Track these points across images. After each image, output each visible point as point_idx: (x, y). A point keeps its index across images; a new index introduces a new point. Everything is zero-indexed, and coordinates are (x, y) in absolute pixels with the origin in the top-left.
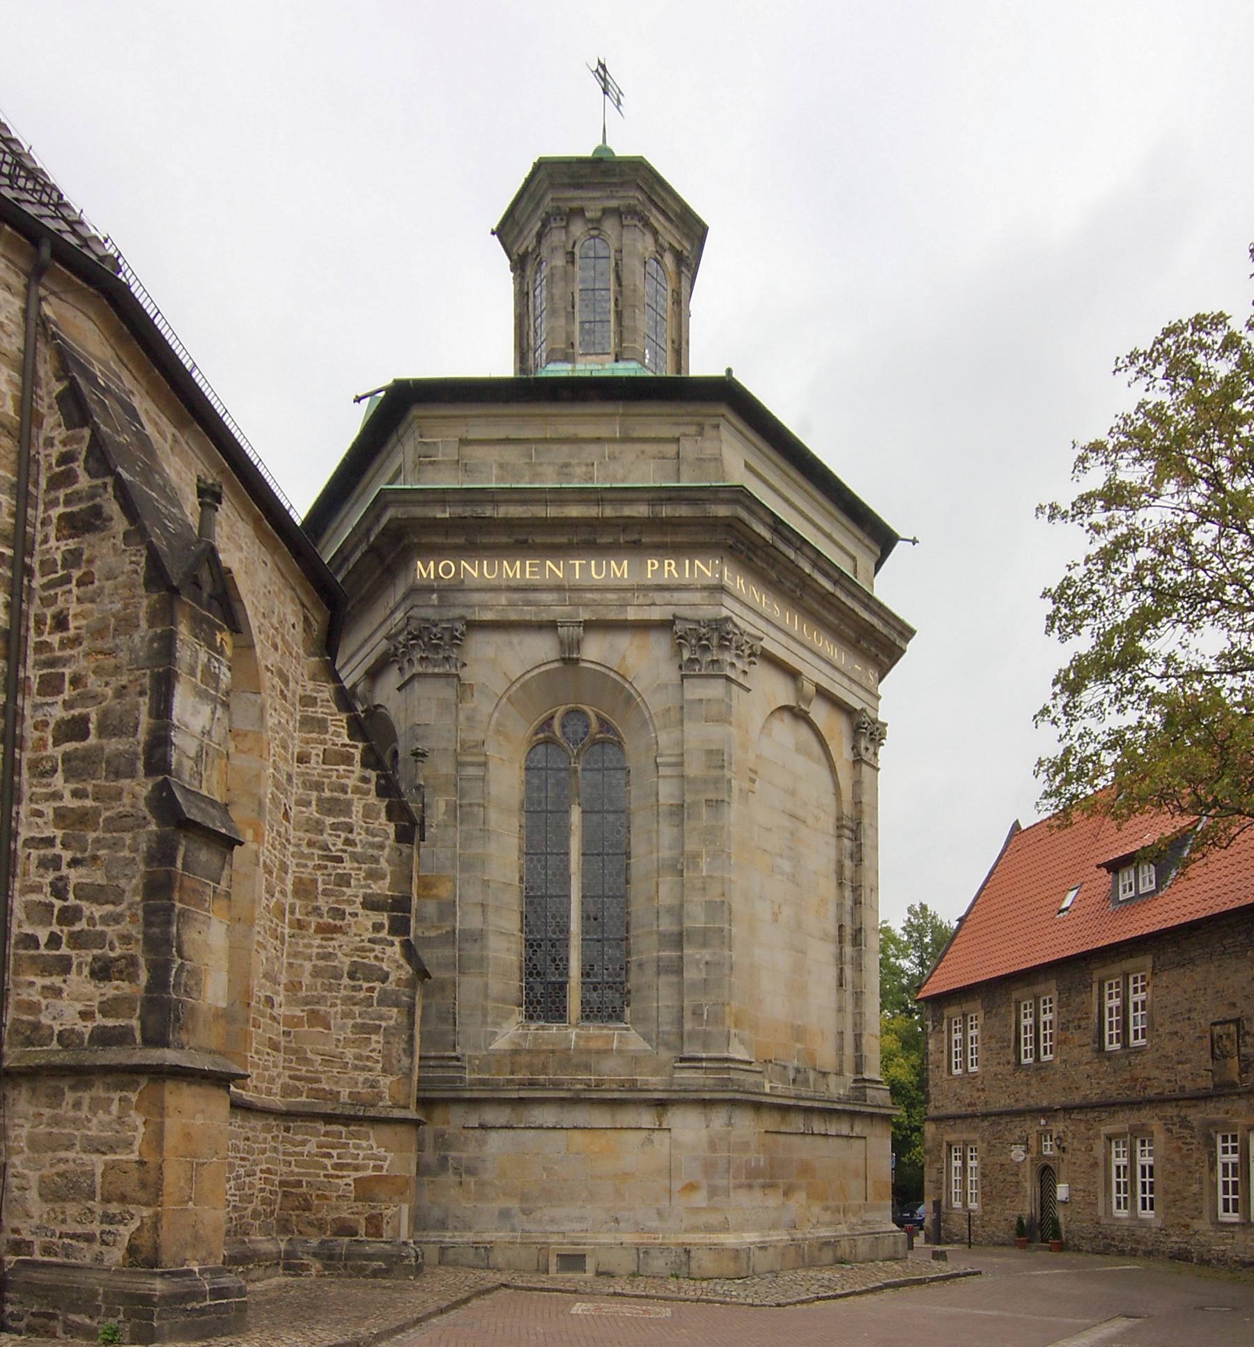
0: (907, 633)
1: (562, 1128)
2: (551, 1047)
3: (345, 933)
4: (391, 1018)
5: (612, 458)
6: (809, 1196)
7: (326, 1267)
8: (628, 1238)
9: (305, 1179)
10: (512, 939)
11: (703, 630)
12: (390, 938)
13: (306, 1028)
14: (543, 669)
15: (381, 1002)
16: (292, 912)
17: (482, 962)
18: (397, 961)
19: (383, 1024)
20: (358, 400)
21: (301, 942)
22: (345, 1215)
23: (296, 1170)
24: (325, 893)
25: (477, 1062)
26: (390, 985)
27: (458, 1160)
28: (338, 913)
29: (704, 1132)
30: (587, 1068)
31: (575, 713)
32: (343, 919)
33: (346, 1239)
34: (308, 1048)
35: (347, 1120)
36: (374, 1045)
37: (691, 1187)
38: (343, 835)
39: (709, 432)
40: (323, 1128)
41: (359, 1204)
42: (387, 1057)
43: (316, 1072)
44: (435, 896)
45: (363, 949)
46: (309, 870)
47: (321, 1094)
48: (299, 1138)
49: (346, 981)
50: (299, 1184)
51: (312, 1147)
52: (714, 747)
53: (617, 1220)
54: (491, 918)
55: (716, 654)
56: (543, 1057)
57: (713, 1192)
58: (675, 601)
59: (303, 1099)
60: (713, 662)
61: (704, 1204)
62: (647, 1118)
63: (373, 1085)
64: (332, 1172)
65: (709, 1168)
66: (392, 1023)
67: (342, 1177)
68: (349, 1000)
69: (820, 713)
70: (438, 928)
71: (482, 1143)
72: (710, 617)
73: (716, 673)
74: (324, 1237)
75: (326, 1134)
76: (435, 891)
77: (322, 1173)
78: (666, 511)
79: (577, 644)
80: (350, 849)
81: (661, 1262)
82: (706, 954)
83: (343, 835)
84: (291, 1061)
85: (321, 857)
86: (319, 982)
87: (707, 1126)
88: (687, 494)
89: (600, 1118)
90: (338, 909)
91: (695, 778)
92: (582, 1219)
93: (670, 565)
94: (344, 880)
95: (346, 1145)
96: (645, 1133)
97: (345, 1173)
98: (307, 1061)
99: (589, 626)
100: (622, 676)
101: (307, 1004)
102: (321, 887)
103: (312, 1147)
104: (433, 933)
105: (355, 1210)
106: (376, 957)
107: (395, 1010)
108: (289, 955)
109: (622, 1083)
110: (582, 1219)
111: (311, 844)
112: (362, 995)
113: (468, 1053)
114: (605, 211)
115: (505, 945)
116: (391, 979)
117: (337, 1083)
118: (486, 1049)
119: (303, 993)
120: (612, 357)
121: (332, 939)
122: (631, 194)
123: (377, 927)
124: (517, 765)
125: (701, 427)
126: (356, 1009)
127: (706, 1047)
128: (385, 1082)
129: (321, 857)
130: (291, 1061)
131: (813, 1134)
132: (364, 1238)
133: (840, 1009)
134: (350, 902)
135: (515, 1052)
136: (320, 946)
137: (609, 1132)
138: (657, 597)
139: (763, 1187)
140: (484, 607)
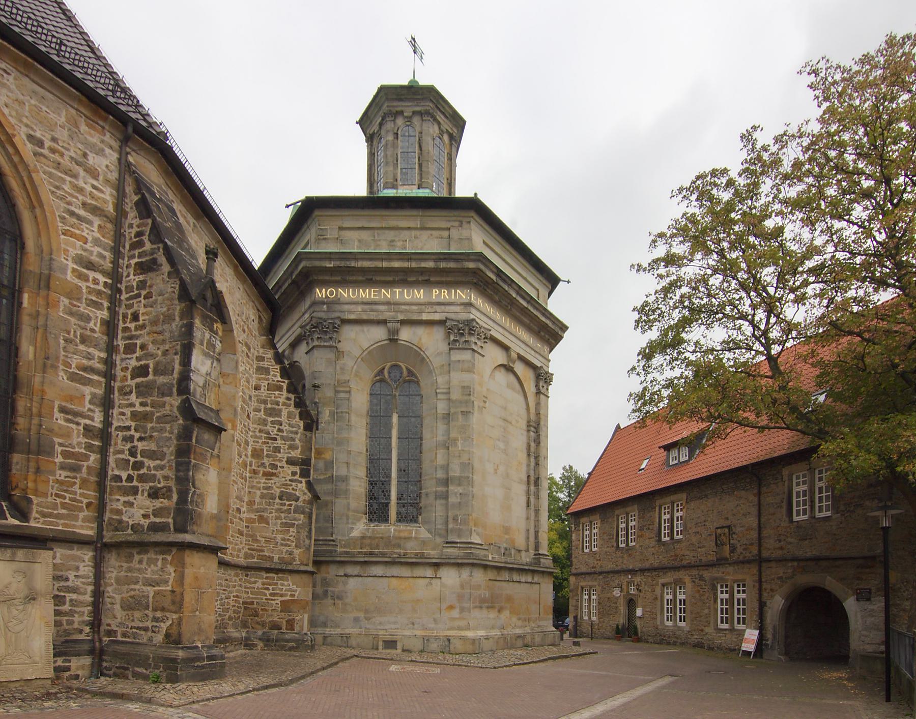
0: (564, 328)
5: (416, 237)
6: (511, 613)
16: (251, 465)
17: (346, 492)
20: (287, 206)
24: (268, 456)
26: (300, 503)
27: (333, 592)
28: (274, 466)
29: (458, 579)
30: (399, 546)
34: (258, 534)
35: (278, 571)
37: (451, 607)
40: (265, 575)
42: (298, 539)
44: (324, 458)
45: (286, 485)
48: (253, 580)
49: (277, 500)
50: (252, 603)
51: (259, 584)
54: (352, 469)
55: (467, 338)
57: (462, 610)
59: (255, 560)
60: (466, 341)
61: (457, 616)
62: (429, 572)
65: (460, 597)
66: (301, 522)
69: (519, 368)
71: (345, 584)
75: (267, 578)
78: (443, 265)
79: (397, 332)
85: (266, 438)
86: (264, 501)
89: (405, 572)
94: (277, 450)
99: (403, 322)
102: (265, 453)
103: (259, 584)
104: (322, 477)
109: (417, 554)
110: (395, 623)
111: (260, 431)
112: (286, 508)
113: (339, 538)
114: (414, 113)
115: (359, 483)
119: (256, 507)
123: (294, 474)
125: (461, 222)
126: (283, 515)
127: (459, 536)
128: (297, 552)
129: (266, 438)
134: (280, 461)
135: (363, 538)
137: (410, 579)
138: (438, 308)
140: (350, 312)
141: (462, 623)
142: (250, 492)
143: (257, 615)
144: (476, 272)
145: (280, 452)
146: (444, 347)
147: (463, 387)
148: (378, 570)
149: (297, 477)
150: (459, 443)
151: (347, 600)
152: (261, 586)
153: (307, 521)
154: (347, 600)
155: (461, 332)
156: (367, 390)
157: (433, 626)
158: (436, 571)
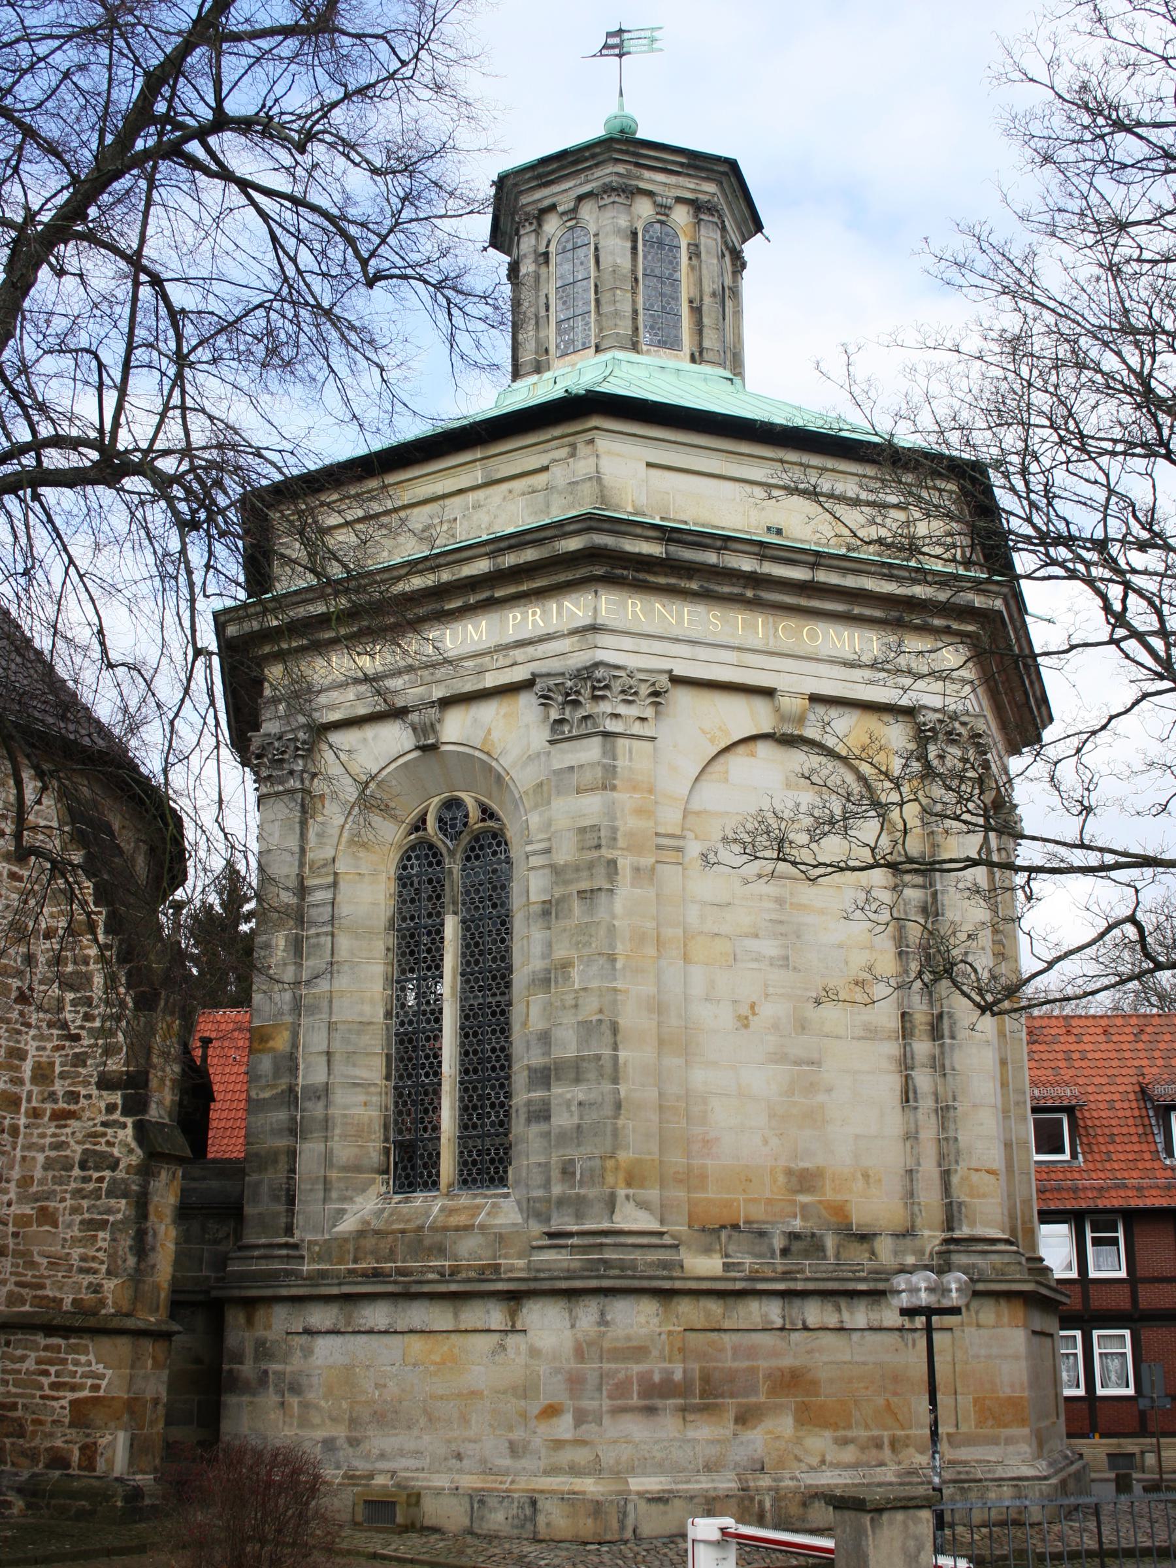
1: (395, 1332)
2: (401, 1226)
3: (79, 1119)
4: (119, 1211)
5: (477, 506)
6: (800, 1422)
7: (29, 1506)
8: (469, 1482)
9: (20, 1401)
10: (372, 1089)
11: (569, 684)
12: (123, 1119)
13: (35, 1228)
14: (401, 761)
15: (110, 1194)
16: (29, 1100)
17: (326, 1124)
18: (128, 1145)
19: (111, 1219)
21: (36, 1132)
22: (59, 1443)
23: (14, 1390)
24: (62, 1076)
25: (317, 1248)
26: (120, 1174)
27: (280, 1375)
28: (73, 1097)
29: (568, 1333)
30: (441, 1251)
31: (453, 804)
32: (77, 1103)
33: (57, 1473)
34: (35, 1250)
35: (66, 1331)
36: (100, 1244)
37: (551, 1412)
38: (83, 1010)
39: (582, 449)
40: (42, 1341)
41: (73, 1431)
42: (112, 1256)
43: (42, 1276)
44: (272, 1049)
45: (95, 1135)
46: (48, 1053)
47: (44, 1302)
48: (19, 1352)
49: (77, 1172)
50: (14, 1406)
51: (30, 1364)
52: (588, 822)
53: (459, 1457)
54: (339, 1067)
55: (589, 708)
56: (391, 1238)
57: (581, 1418)
58: (539, 654)
59: (27, 1308)
60: (586, 718)
61: (568, 1436)
62: (496, 1316)
63: (96, 1289)
64: (48, 1392)
65: (575, 1383)
66: (120, 1216)
67: (57, 1399)
68: (78, 1193)
70: (273, 1086)
71: (308, 1352)
72: (579, 666)
73: (589, 728)
74: (36, 1470)
75: (46, 1348)
76: (271, 1044)
77: (38, 1393)
78: (510, 560)
79: (431, 728)
80: (88, 1025)
81: (499, 1516)
82: (578, 1093)
83: (83, 1010)
84: (18, 1266)
85: (60, 1037)
86: (50, 1174)
87: (573, 1326)
88: (528, 537)
89: (438, 1317)
90: (73, 1093)
91: (565, 865)
92: (417, 1454)
93: (534, 614)
94: (80, 1060)
95: (64, 1362)
96: (497, 1336)
97: (61, 1394)
98: (32, 1265)
99: (446, 703)
100: (488, 754)
101: (37, 1200)
102: (58, 1069)
103: (30, 1364)
104: (266, 1094)
105: (68, 1438)
106: (108, 1143)
107: (124, 1201)
108: (24, 1148)
109: (482, 1269)
110: (417, 1454)
111: (50, 1025)
112: (92, 1186)
113: (309, 1237)
114: (580, 198)
115: (362, 1098)
116: (121, 1166)
117: (60, 1289)
118: (329, 1232)
119: (34, 1189)
120: (593, 349)
121: (65, 1126)
122: (608, 171)
123: (111, 1108)
124: (384, 876)
125: (573, 446)
126: (85, 1203)
127: (579, 1217)
128: (110, 1285)
129: (60, 1037)
130: (18, 1266)
131: (806, 1328)
132: (77, 1472)
133: (911, 1137)
134: (86, 1083)
135: (361, 1234)
136: (54, 1135)
137: (453, 1336)
138: (519, 654)
139: (684, 1409)
140: (331, 707)
141: (581, 1456)
142: (24, 1158)
143: (22, 1435)
144: (592, 555)
145: (85, 1065)
146: (540, 736)
147: (582, 830)
148: (376, 1315)
149: (116, 1116)
150: (575, 973)
151: (311, 1396)
152: (34, 1367)
153: (131, 1213)
154: (311, 1396)
155: (575, 697)
156: (392, 870)
157: (507, 1462)
158: (513, 1315)
